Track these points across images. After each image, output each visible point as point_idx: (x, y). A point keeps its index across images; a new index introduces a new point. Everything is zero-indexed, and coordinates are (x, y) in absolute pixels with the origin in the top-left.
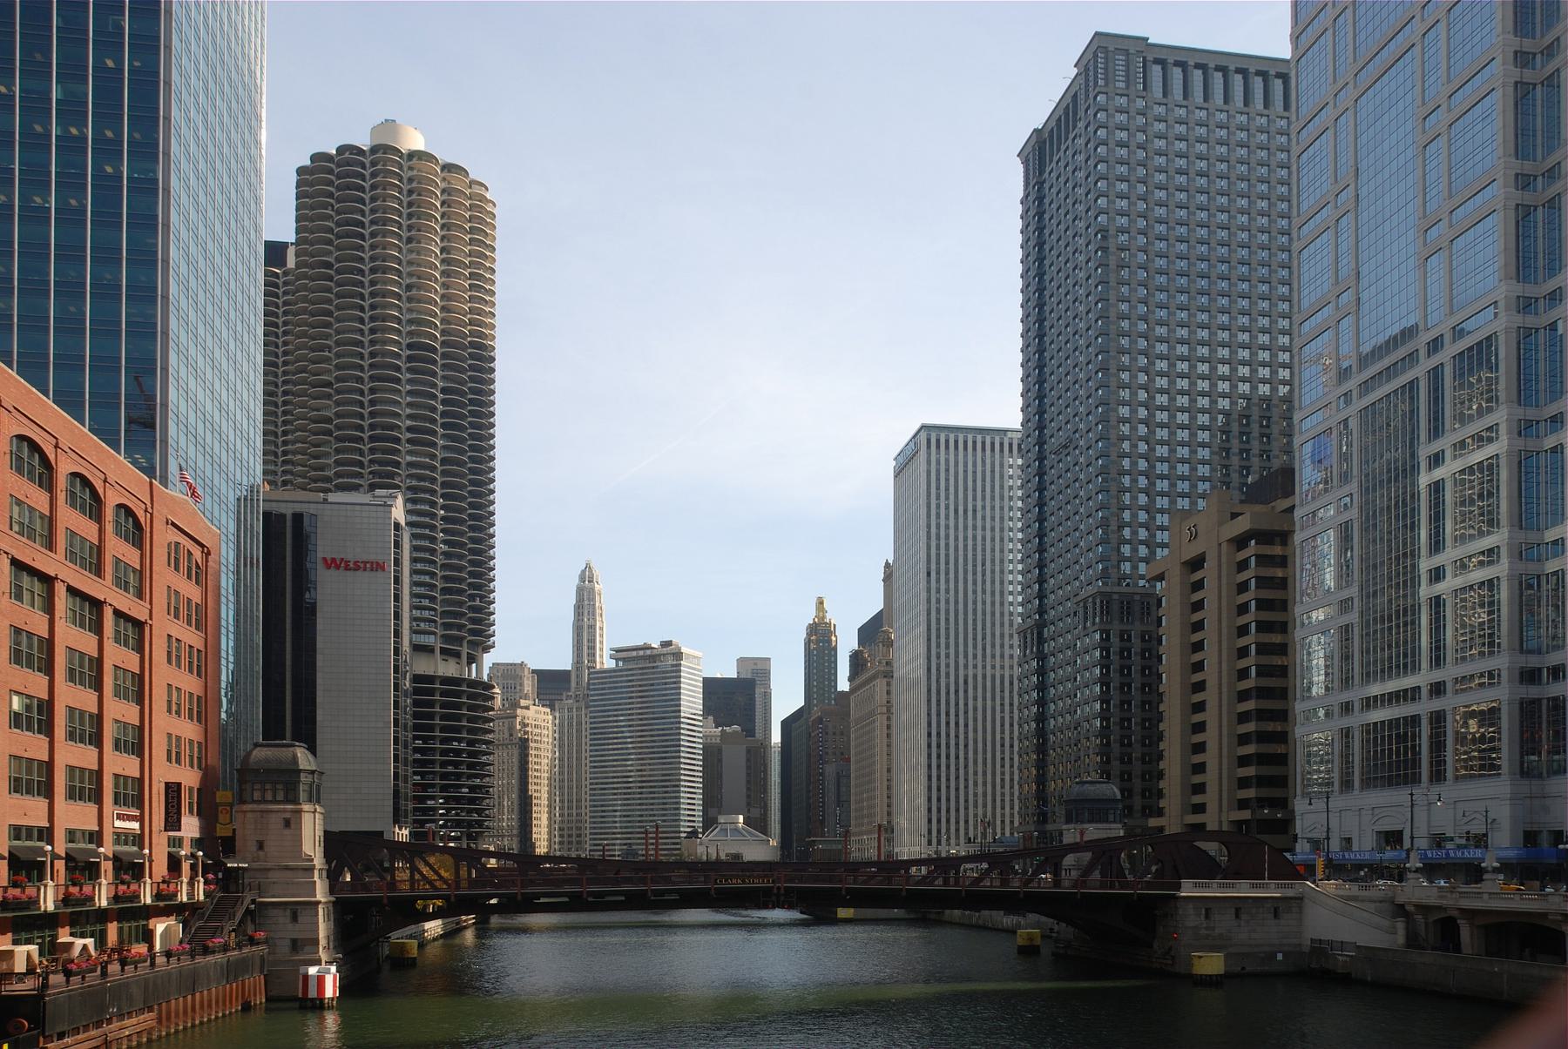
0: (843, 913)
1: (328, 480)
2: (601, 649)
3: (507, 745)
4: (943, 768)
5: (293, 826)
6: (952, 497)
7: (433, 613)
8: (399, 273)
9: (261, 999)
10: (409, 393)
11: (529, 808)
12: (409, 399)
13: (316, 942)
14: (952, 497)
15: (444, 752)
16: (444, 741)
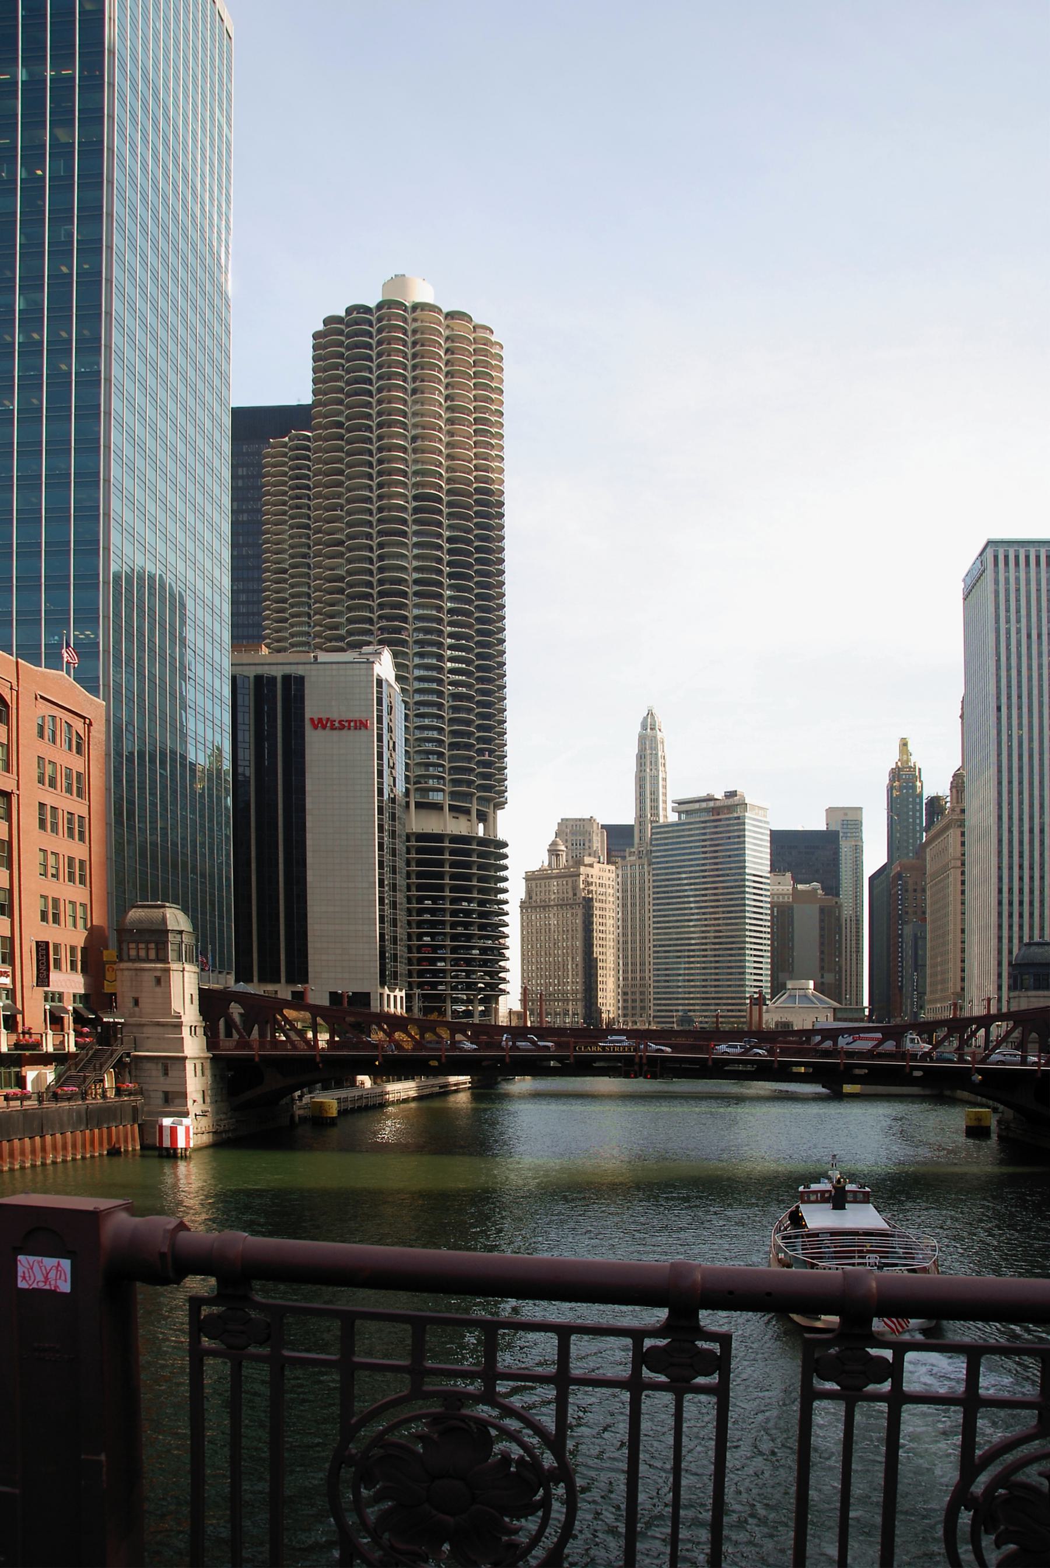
0: (848, 1088)
1: (341, 638)
2: (665, 802)
3: (571, 905)
4: (1016, 928)
5: (163, 984)
6: (1024, 620)
7: (441, 769)
8: (404, 426)
9: (134, 1146)
10: (416, 545)
11: (593, 971)
12: (416, 551)
13: (184, 1095)
14: (1024, 620)
15: (454, 913)
16: (454, 901)
